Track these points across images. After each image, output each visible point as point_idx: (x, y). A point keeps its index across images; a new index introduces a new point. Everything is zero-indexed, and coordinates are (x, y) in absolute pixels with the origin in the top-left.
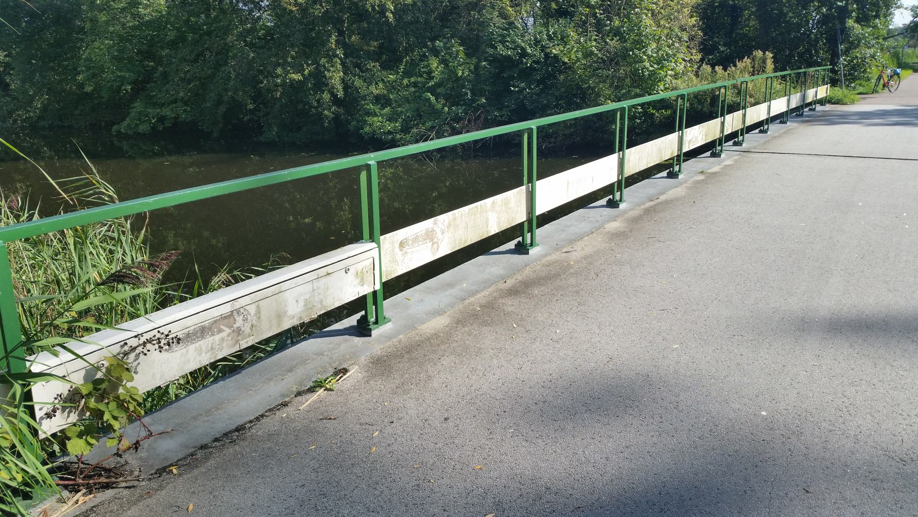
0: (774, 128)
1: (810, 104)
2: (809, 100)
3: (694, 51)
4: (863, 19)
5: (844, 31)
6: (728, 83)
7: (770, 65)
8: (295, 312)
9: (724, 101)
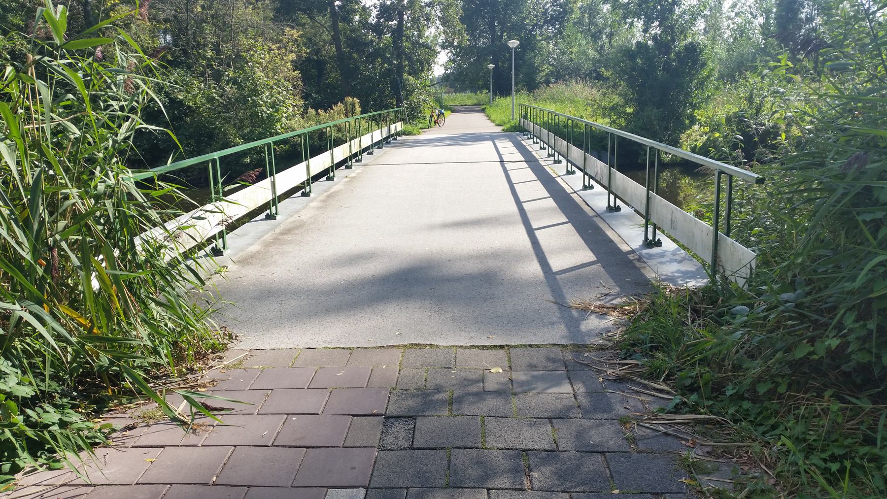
0: (339, 174)
1: (393, 135)
2: (392, 132)
3: (297, 98)
4: (414, 73)
5: (402, 81)
6: (331, 124)
7: (358, 109)
8: (241, 212)
9: (330, 136)
